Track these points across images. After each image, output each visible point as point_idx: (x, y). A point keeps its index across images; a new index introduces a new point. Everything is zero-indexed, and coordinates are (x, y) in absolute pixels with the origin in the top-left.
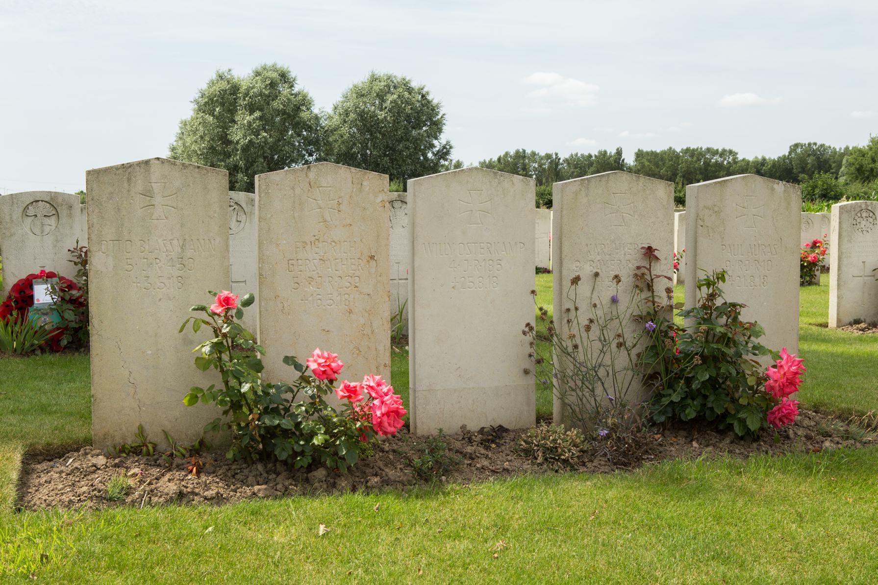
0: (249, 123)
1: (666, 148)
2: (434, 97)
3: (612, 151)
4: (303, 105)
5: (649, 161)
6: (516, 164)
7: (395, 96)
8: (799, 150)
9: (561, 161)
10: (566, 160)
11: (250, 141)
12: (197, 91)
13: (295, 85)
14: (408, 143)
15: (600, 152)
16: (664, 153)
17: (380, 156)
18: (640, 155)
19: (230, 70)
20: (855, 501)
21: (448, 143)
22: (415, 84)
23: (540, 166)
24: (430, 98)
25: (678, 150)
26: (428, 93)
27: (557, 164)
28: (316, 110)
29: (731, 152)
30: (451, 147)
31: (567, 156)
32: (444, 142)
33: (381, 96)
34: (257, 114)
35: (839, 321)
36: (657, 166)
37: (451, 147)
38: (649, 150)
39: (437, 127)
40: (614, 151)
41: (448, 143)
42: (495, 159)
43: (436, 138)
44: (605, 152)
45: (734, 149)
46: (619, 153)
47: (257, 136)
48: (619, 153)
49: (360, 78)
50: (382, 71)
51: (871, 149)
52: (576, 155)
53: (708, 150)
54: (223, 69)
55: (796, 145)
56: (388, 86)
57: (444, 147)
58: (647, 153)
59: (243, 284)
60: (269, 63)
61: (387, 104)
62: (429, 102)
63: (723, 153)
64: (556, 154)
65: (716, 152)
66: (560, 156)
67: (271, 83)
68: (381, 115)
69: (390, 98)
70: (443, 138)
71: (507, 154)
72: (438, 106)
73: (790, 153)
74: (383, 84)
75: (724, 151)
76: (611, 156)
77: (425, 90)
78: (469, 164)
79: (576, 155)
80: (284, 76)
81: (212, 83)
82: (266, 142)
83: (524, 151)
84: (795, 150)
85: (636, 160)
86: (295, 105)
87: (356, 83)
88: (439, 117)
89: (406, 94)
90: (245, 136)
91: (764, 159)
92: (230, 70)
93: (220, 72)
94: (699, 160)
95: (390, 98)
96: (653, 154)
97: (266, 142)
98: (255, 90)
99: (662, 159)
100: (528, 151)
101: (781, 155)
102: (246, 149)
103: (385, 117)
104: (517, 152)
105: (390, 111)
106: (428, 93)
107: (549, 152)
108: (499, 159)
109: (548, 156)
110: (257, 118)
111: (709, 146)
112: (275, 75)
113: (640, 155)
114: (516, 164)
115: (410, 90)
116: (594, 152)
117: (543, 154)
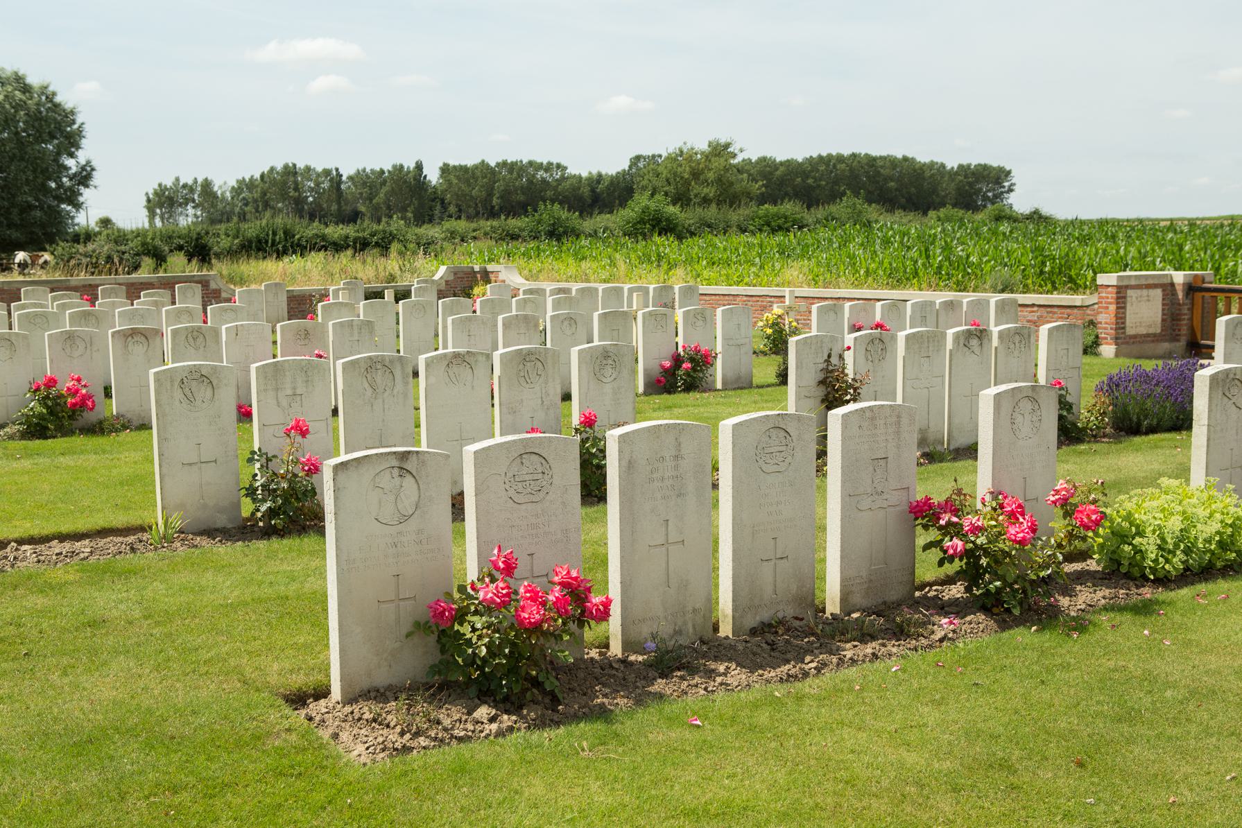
1: (477, 161)
2: (66, 98)
3: (410, 164)
5: (458, 178)
6: (285, 183)
8: (641, 165)
9: (344, 178)
10: (350, 178)
14: (23, 164)
15: (394, 167)
16: (476, 167)
18: (445, 170)
21: (88, 162)
22: (34, 80)
23: (318, 184)
24: (58, 99)
25: (493, 164)
26: (54, 94)
27: (340, 182)
29: (559, 166)
30: (93, 169)
31: (352, 172)
32: (83, 162)
35: (724, 383)
36: (467, 182)
37: (93, 169)
38: (457, 164)
39: (72, 141)
40: (412, 166)
41: (88, 162)
42: (257, 176)
43: (72, 155)
44: (402, 167)
45: (564, 163)
46: (419, 167)
48: (419, 167)
52: (364, 170)
53: (531, 163)
55: (638, 158)
57: (83, 168)
58: (454, 167)
62: (57, 106)
63: (548, 168)
64: (337, 170)
65: (540, 166)
66: (341, 172)
70: (82, 156)
71: (272, 169)
72: (72, 113)
73: (630, 167)
75: (550, 164)
76: (409, 172)
77: (51, 89)
78: (221, 183)
79: (364, 170)
83: (294, 165)
84: (635, 164)
85: (441, 176)
88: (75, 127)
91: (600, 175)
94: (520, 176)
96: (463, 169)
99: (474, 176)
100: (301, 165)
101: (619, 169)
104: (286, 167)
106: (54, 94)
107: (328, 167)
108: (262, 176)
109: (327, 172)
111: (532, 158)
113: (445, 170)
114: (285, 183)
115: (26, 89)
116: (387, 167)
117: (319, 169)
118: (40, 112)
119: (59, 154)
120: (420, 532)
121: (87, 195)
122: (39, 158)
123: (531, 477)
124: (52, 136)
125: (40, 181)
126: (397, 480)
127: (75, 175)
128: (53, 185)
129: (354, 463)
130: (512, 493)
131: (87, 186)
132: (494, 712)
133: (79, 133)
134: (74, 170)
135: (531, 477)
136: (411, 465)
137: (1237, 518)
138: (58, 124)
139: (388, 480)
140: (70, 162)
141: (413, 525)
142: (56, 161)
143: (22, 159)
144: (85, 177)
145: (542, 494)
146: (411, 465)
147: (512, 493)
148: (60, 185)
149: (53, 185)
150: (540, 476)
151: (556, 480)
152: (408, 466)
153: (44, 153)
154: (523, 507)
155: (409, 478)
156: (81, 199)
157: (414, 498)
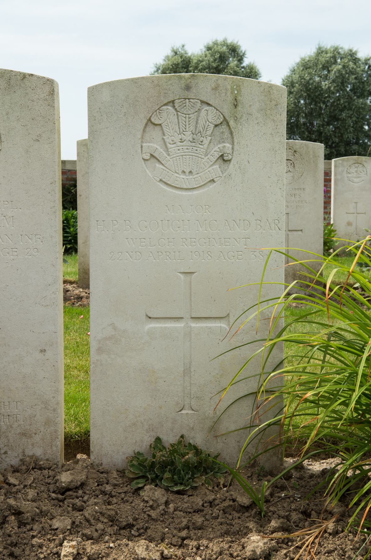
7: (340, 67)
12: (153, 66)
13: (245, 59)
17: (323, 126)
19: (183, 46)
20: (302, 82)
33: (326, 66)
49: (308, 51)
50: (328, 45)
54: (177, 45)
56: (334, 57)
59: (300, 233)
60: (220, 39)
61: (332, 76)
67: (220, 57)
68: (325, 84)
69: (335, 68)
74: (329, 55)
80: (234, 50)
81: (167, 57)
87: (303, 56)
89: (351, 64)
92: (183, 46)
93: (175, 48)
95: (335, 68)
98: (204, 63)
103: (329, 88)
105: (334, 81)
112: (224, 49)
143: (350, 109)
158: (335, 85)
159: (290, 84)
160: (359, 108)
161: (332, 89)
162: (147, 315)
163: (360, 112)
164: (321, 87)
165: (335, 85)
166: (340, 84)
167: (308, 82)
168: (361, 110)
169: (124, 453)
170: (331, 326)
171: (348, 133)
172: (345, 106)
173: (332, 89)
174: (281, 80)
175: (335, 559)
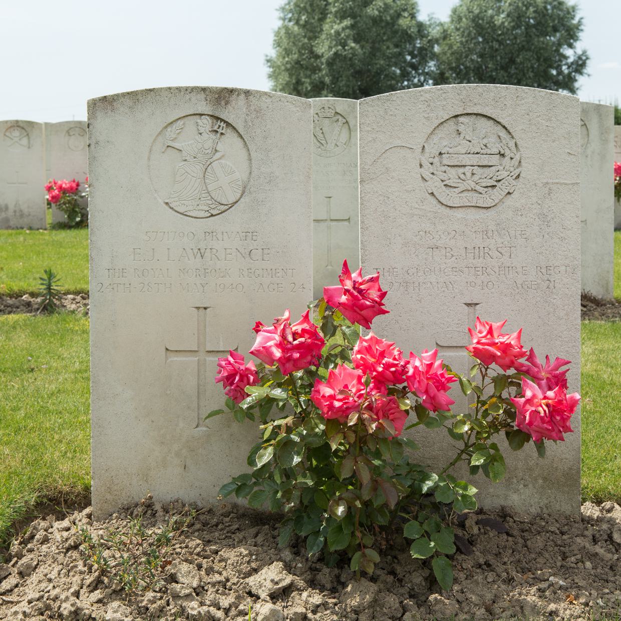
0: (338, 33)
4: (405, 10)
11: (336, 54)
21: (584, 52)
28: (422, 17)
30: (587, 58)
32: (579, 52)
34: (347, 22)
39: (571, 34)
41: (584, 52)
43: (571, 46)
47: (344, 47)
51: (445, 36)
57: (580, 58)
70: (579, 47)
82: (354, 55)
86: (396, 11)
87: (420, 13)
90: (330, 48)
97: (354, 55)
102: (330, 63)
103: (503, 23)
110: (347, 27)
118: (547, 10)
119: (560, 45)
120: (248, 235)
121: (581, 81)
122: (543, 49)
123: (475, 160)
124: (555, 30)
125: (542, 68)
126: (209, 139)
127: (572, 63)
128: (554, 72)
129: (128, 102)
130: (435, 184)
131: (581, 73)
132: (288, 579)
133: (577, 27)
134: (571, 60)
135: (475, 160)
136: (234, 113)
137: (443, 613)
138: (561, 19)
139: (194, 137)
140: (568, 52)
141: (235, 221)
142: (557, 51)
143: (529, 50)
144: (580, 65)
145: (497, 194)
146: (234, 113)
147: (435, 184)
148: (560, 72)
149: (554, 72)
150: (495, 160)
151: (527, 170)
152: (227, 114)
153: (547, 45)
154: (459, 214)
155: (230, 135)
156: (576, 85)
157: (241, 174)
158: (509, 19)
159: (456, 16)
160: (540, 49)
161: (506, 24)
162: (437, 344)
163: (541, 54)
164: (493, 22)
165: (509, 19)
166: (516, 19)
167: (477, 16)
168: (542, 51)
169: (122, 504)
170: (406, 429)
171: (526, 79)
172: (523, 46)
173: (506, 24)
174: (449, 13)
175: (1, 390)
